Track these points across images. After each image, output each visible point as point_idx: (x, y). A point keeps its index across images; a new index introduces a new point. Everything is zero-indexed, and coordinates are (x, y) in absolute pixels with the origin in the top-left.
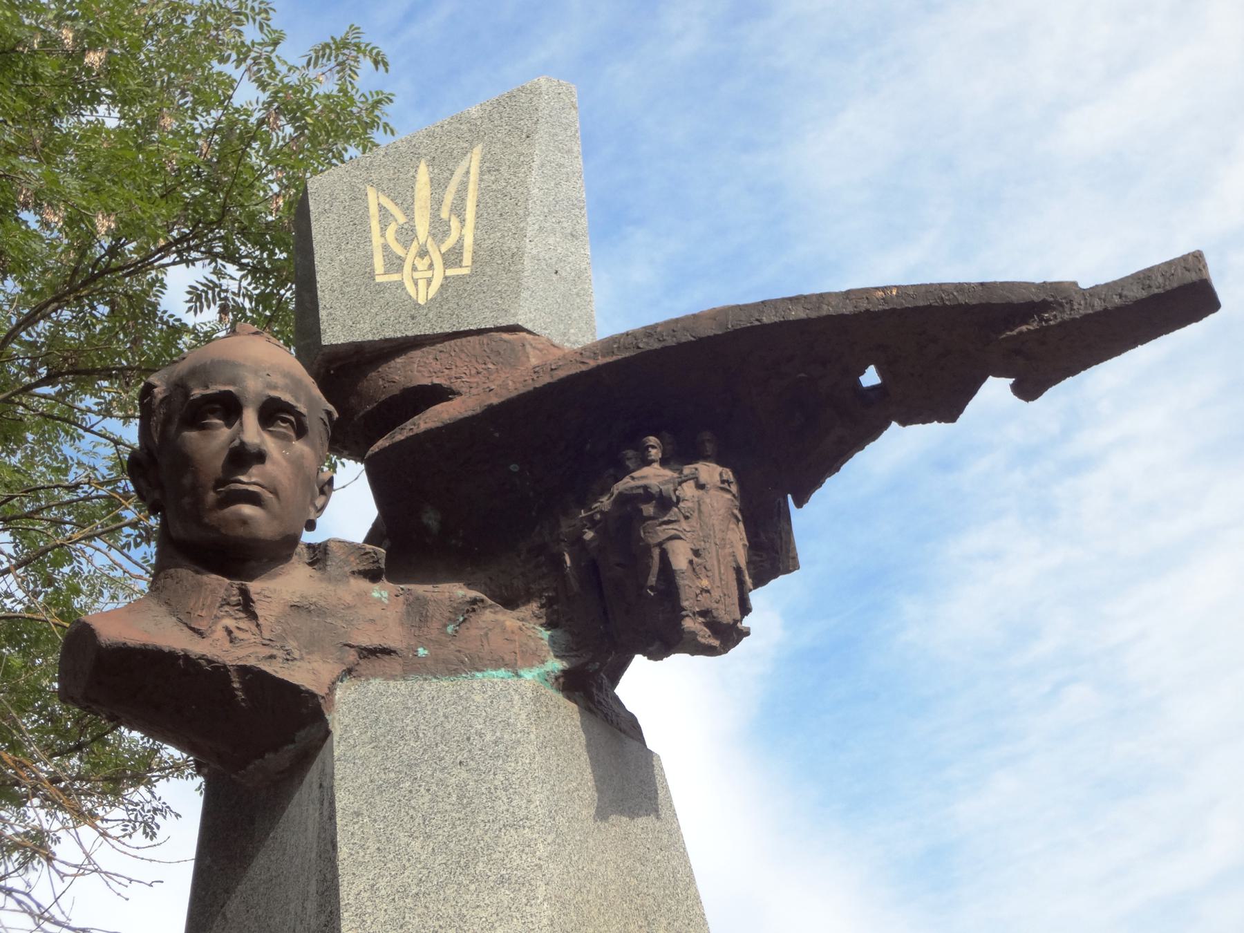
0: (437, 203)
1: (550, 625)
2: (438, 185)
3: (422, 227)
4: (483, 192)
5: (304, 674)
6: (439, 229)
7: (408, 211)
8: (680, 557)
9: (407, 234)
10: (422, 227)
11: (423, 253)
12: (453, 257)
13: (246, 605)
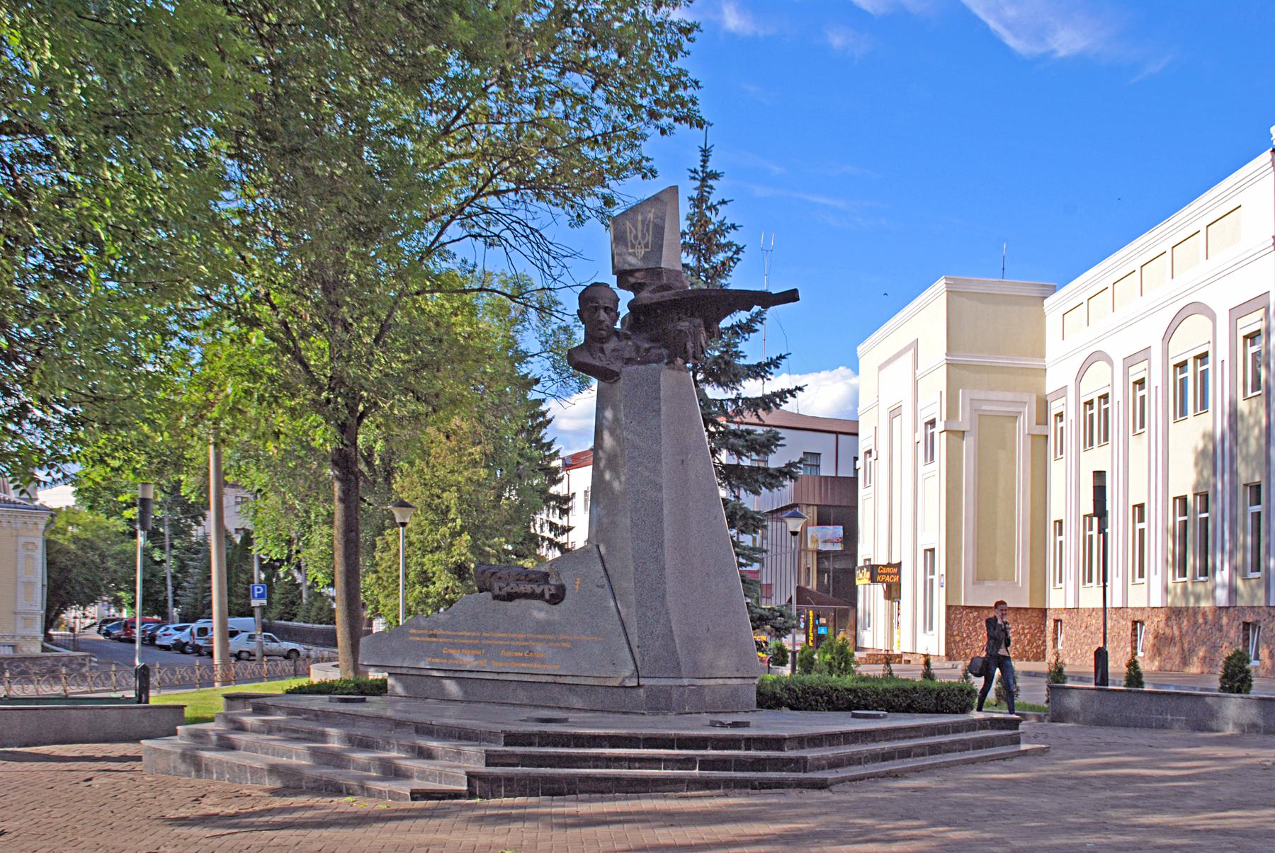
6: (643, 238)
9: (636, 237)
12: (646, 246)
13: (602, 350)
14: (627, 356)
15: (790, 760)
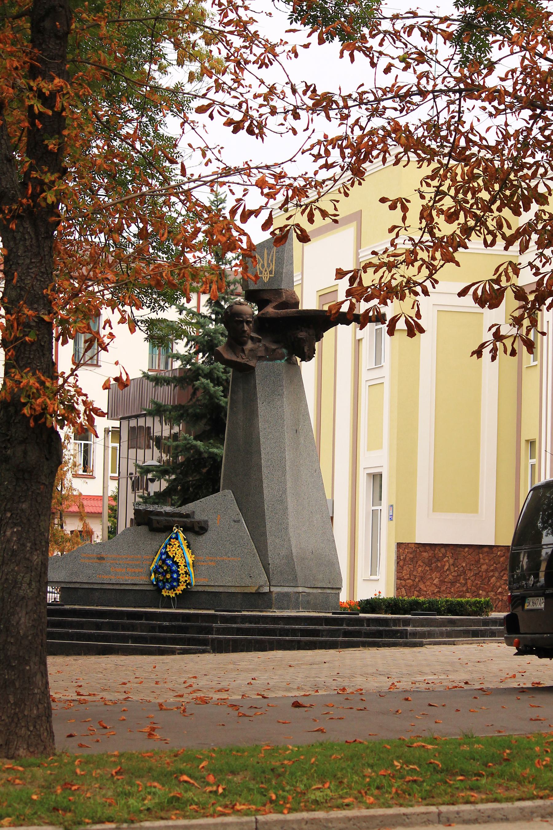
0: (268, 259)
1: (285, 348)
2: (268, 255)
3: (266, 265)
4: (276, 257)
5: (252, 364)
6: (269, 266)
7: (263, 260)
8: (306, 351)
9: (263, 266)
10: (266, 265)
11: (266, 271)
12: (271, 272)
14: (260, 354)
15: (398, 631)
